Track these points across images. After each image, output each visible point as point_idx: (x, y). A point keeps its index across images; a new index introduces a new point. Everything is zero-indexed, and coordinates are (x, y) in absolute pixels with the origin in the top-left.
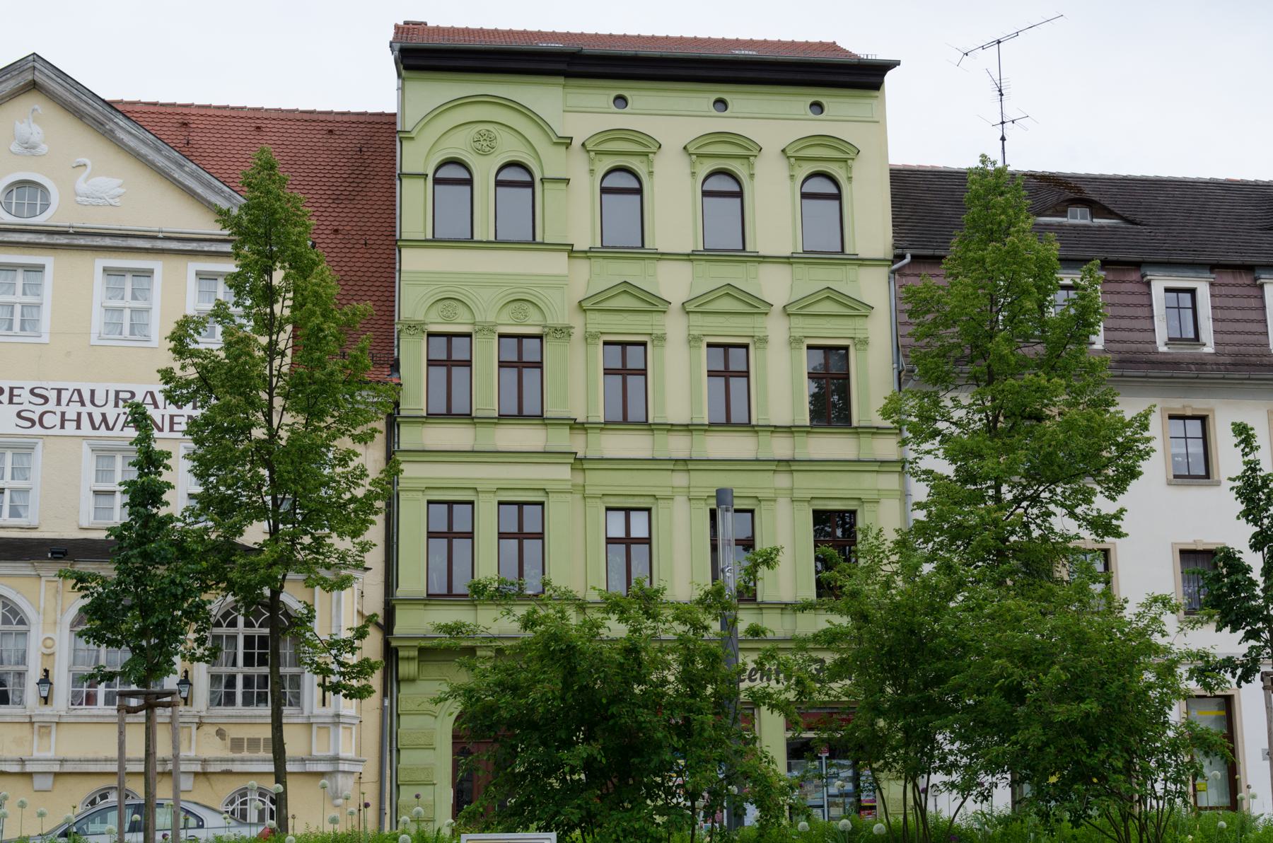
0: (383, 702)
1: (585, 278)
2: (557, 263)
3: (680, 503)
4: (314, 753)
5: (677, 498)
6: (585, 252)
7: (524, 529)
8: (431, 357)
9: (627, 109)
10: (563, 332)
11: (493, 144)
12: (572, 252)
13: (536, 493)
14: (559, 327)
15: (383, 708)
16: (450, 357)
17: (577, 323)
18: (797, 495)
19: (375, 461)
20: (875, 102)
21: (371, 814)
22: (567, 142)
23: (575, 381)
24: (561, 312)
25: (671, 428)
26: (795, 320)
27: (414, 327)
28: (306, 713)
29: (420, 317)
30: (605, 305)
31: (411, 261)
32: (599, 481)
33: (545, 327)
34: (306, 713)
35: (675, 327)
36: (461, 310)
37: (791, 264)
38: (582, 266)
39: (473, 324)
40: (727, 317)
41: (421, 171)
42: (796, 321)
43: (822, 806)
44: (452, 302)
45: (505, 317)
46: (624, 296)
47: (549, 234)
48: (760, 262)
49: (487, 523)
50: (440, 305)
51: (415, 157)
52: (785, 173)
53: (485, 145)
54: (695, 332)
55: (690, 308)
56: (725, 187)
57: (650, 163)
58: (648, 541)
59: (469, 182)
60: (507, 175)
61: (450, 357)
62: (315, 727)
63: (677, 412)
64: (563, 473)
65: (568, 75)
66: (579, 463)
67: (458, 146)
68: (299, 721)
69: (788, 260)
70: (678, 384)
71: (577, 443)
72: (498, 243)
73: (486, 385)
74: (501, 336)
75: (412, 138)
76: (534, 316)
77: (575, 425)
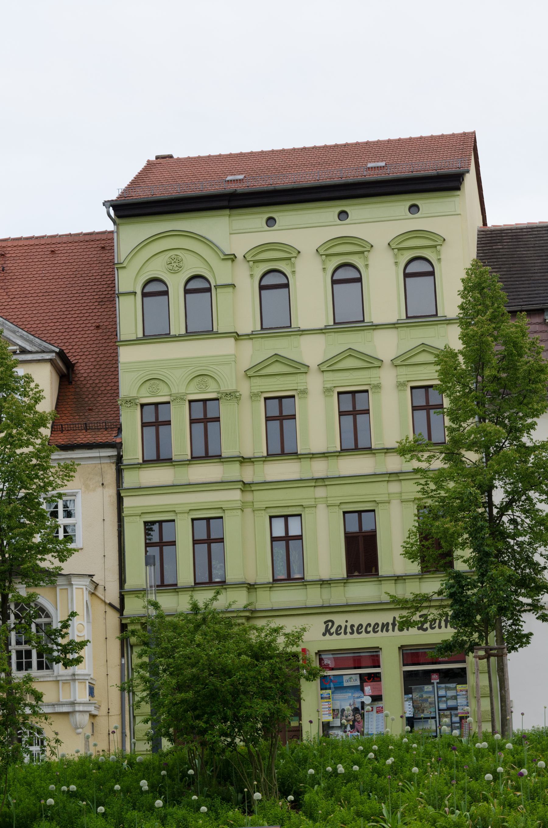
0: (121, 661)
1: (250, 353)
2: (226, 346)
3: (321, 509)
4: (61, 700)
5: (392, 501)
6: (248, 335)
7: (209, 537)
8: (193, 418)
9: (276, 227)
10: (233, 396)
11: (181, 264)
12: (237, 337)
13: (216, 511)
14: (228, 392)
15: (122, 666)
16: (156, 420)
17: (245, 388)
18: (405, 497)
19: (110, 496)
20: (457, 199)
21: (117, 737)
22: (232, 258)
23: (244, 429)
24: (229, 380)
25: (313, 456)
26: (254, 380)
27: (130, 401)
28: (55, 674)
29: (134, 394)
30: (263, 372)
31: (127, 355)
32: (264, 498)
33: (218, 393)
34: (55, 674)
35: (388, 377)
36: (162, 386)
37: (397, 328)
38: (247, 346)
39: (170, 395)
40: (351, 372)
41: (131, 290)
42: (403, 370)
43: (435, 718)
44: (156, 381)
45: (193, 388)
46: (277, 364)
47: (221, 326)
48: (374, 329)
49: (183, 535)
50: (148, 384)
51: (128, 280)
52: (392, 261)
53: (175, 266)
54: (328, 386)
55: (250, 373)
56: (346, 276)
57: (439, 253)
58: (300, 538)
59: (166, 293)
60: (193, 285)
61: (156, 420)
62: (61, 683)
63: (318, 447)
64: (236, 495)
65: (231, 208)
66: (246, 486)
67: (157, 269)
68: (51, 679)
69: (394, 326)
70: (317, 424)
71: (249, 474)
72: (190, 334)
73: (180, 438)
74: (190, 402)
75: (124, 267)
76: (164, 390)
77: (243, 460)
